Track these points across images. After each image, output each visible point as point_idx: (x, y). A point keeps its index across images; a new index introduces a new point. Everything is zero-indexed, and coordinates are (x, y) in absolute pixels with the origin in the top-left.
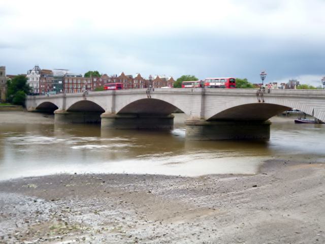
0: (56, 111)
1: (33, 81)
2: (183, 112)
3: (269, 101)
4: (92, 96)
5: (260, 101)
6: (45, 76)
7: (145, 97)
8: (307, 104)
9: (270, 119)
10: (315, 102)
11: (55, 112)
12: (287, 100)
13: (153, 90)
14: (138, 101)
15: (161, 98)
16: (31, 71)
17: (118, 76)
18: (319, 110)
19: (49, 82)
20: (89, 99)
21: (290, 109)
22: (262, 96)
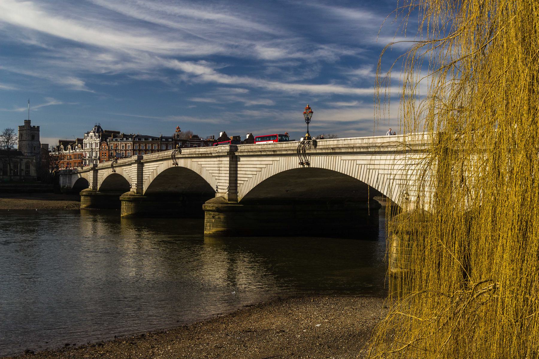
16: (88, 133)
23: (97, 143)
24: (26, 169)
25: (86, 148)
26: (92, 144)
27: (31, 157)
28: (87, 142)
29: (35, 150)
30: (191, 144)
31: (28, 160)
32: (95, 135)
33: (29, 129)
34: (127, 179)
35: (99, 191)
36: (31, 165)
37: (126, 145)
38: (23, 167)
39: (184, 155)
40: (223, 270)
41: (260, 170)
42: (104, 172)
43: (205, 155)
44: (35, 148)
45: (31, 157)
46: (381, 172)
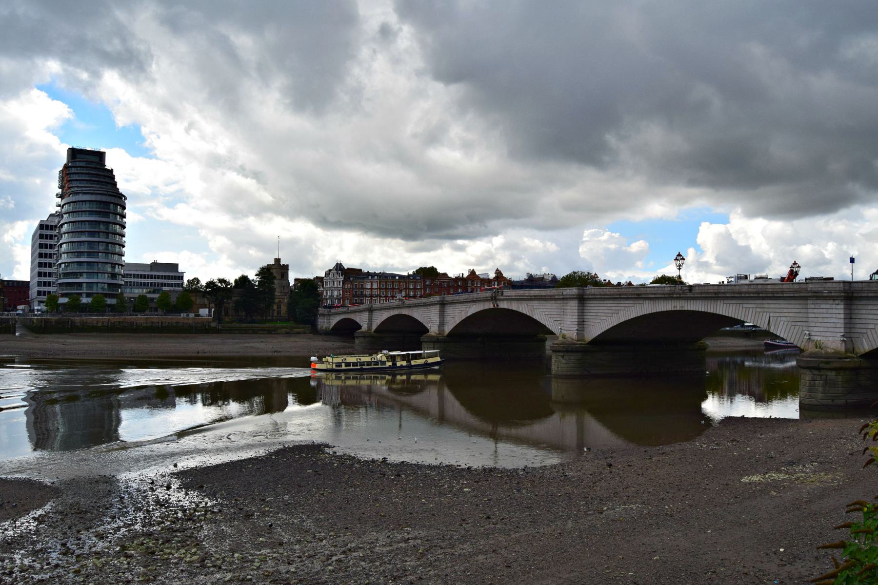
1: (332, 291)
7: (490, 305)
8: (758, 310)
10: (772, 305)
13: (502, 294)
14: (394, 316)
15: (515, 306)
18: (779, 319)
20: (504, 305)
21: (742, 323)
27: (283, 297)
30: (440, 282)
31: (279, 299)
34: (419, 320)
35: (376, 331)
36: (282, 305)
39: (506, 296)
42: (456, 314)
43: (523, 298)
45: (283, 297)
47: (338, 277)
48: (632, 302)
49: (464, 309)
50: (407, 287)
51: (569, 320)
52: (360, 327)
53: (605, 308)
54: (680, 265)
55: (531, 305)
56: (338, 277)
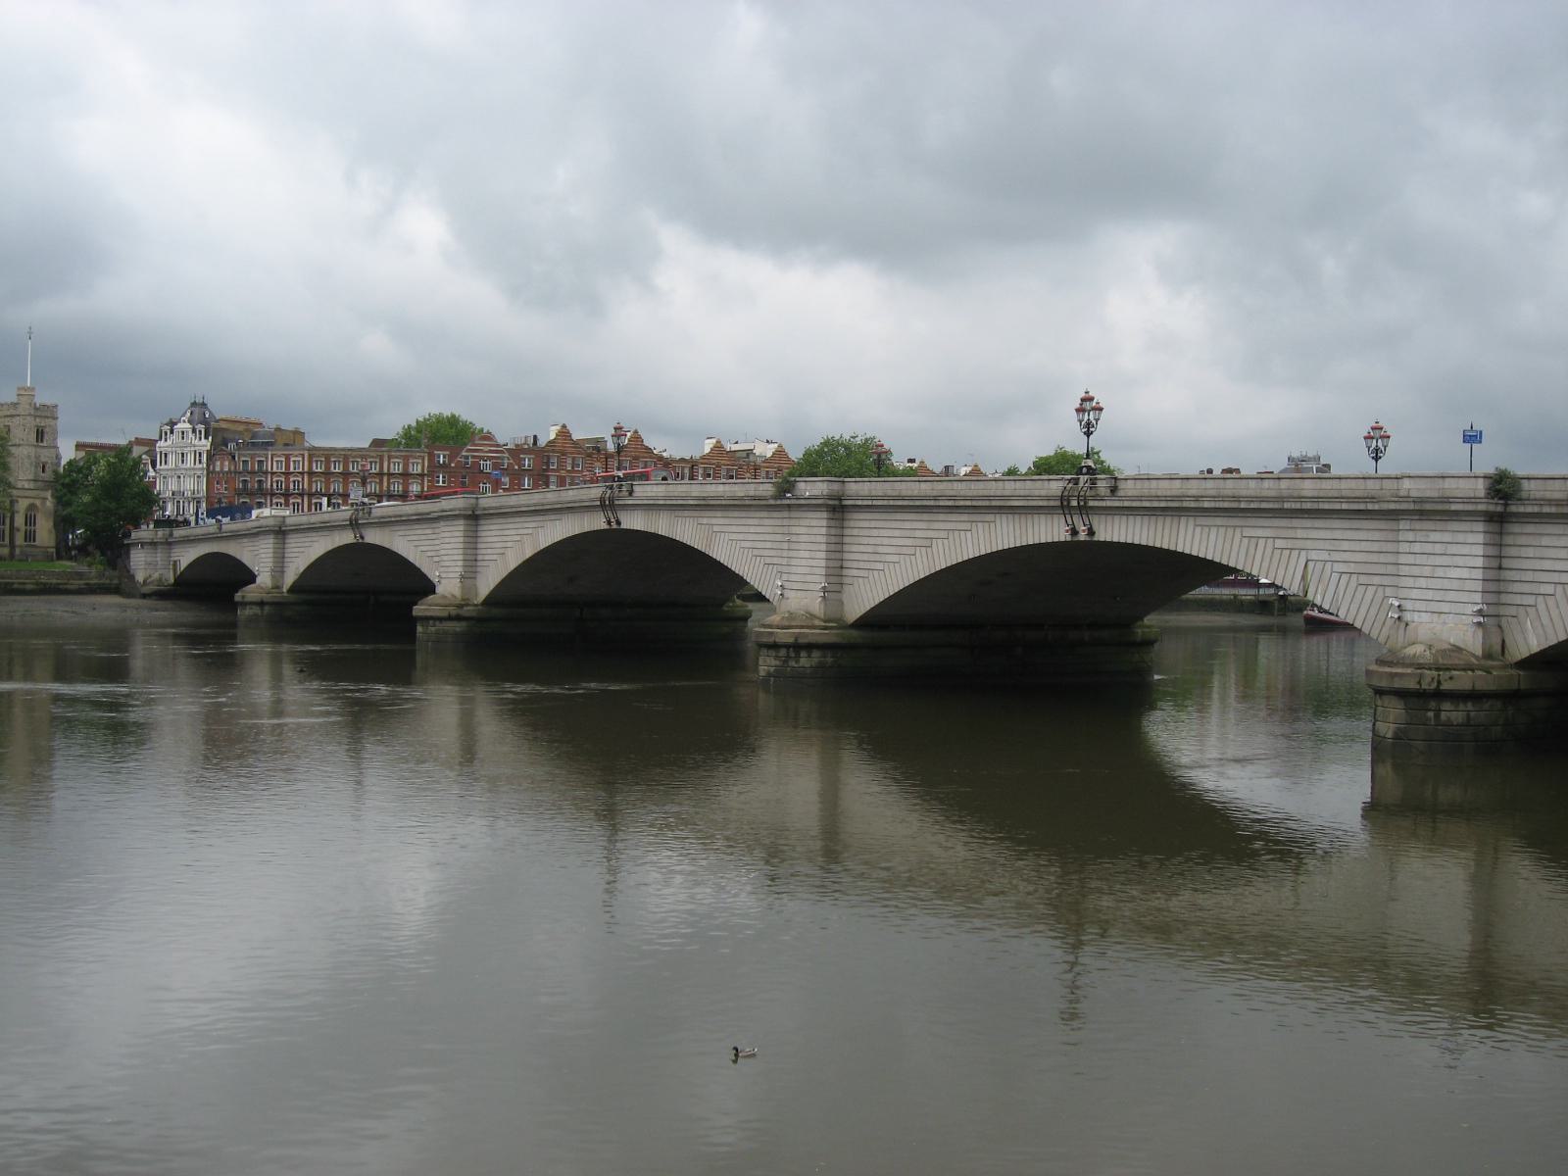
0: (249, 593)
2: (1347, 627)
3: (1114, 531)
4: (385, 523)
5: (1074, 532)
6: (231, 446)
7: (347, 538)
8: (1279, 543)
9: (1147, 621)
11: (238, 597)
12: (1043, 517)
13: (631, 493)
15: (663, 525)
16: (172, 424)
17: (542, 442)
19: (246, 472)
20: (373, 537)
22: (1084, 510)
23: (200, 454)
24: (26, 525)
25: (166, 467)
26: (183, 456)
28: (170, 449)
29: (43, 471)
31: (32, 501)
32: (194, 431)
33: (30, 415)
36: (39, 516)
37: (288, 458)
38: (19, 521)
40: (481, 756)
41: (927, 543)
44: (44, 467)
46: (1313, 555)
47: (197, 442)
48: (965, 517)
49: (530, 531)
50: (385, 471)
51: (804, 562)
52: (251, 578)
53: (897, 533)
54: (1089, 425)
55: (705, 521)
56: (197, 442)
